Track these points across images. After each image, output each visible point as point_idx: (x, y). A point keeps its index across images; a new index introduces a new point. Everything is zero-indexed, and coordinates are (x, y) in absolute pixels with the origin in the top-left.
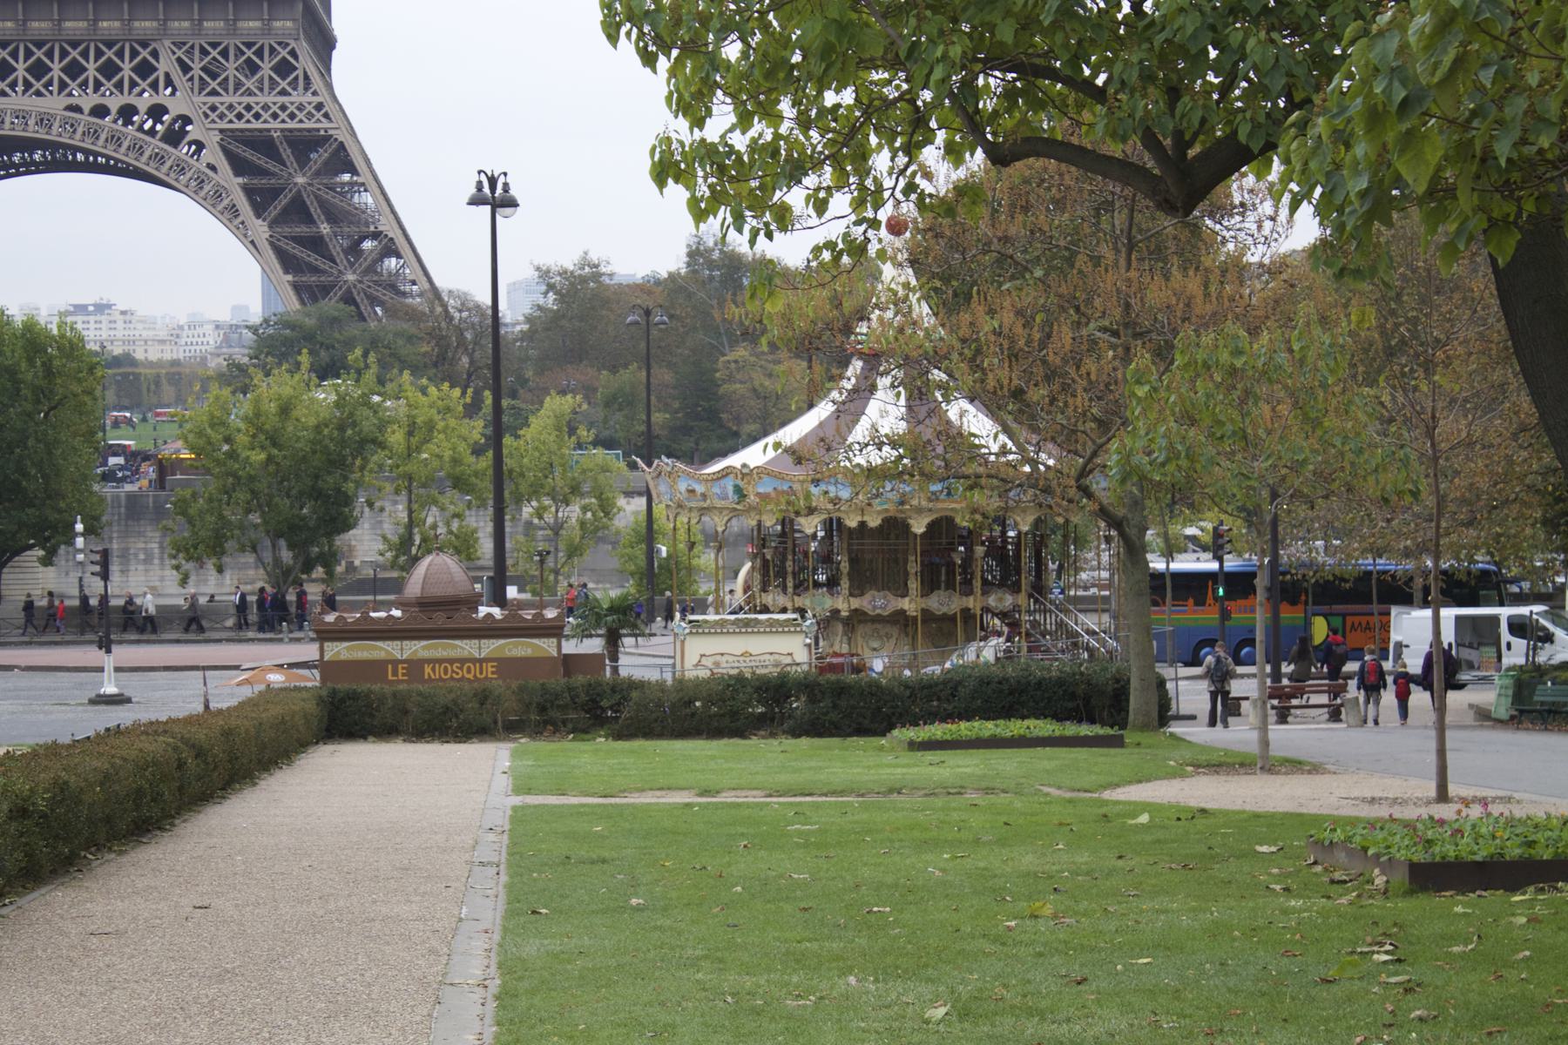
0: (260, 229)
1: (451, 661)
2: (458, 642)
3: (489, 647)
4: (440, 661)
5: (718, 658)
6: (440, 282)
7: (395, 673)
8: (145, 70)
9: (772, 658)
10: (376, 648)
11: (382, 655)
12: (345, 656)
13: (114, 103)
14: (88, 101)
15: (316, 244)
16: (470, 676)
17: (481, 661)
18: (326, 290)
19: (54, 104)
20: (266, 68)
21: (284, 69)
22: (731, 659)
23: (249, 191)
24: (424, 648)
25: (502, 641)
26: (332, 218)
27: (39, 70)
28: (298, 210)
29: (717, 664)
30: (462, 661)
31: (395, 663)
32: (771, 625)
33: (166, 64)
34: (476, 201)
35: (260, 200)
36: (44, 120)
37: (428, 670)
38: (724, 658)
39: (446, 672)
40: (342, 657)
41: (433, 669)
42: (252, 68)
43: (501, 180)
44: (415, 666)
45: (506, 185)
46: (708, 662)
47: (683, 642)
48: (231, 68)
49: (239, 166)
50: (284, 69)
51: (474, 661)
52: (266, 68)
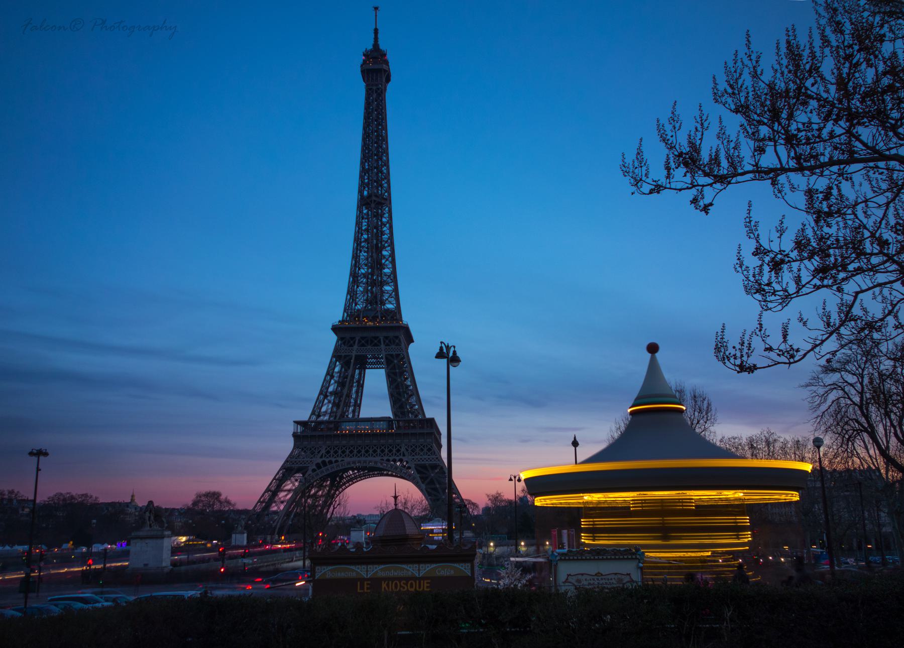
0: (423, 486)
1: (400, 579)
2: (404, 566)
3: (425, 569)
4: (393, 579)
5: (580, 577)
6: (463, 497)
7: (362, 587)
8: (398, 451)
9: (616, 577)
10: (353, 571)
11: (354, 575)
12: (329, 576)
13: (391, 458)
14: (385, 458)
15: (435, 489)
16: (413, 590)
17: (420, 579)
18: (438, 500)
19: (378, 459)
20: (425, 450)
21: (429, 450)
22: (588, 578)
23: (421, 478)
24: (382, 570)
25: (434, 565)
26: (439, 484)
27: (375, 451)
28: (432, 482)
29: (579, 581)
30: (407, 579)
31: (362, 580)
32: (615, 554)
33: (403, 450)
34: (440, 355)
35: (423, 479)
36: (376, 462)
37: (384, 585)
38: (584, 577)
39: (396, 587)
40: (327, 577)
41: (388, 585)
42: (422, 450)
43: (452, 349)
44: (376, 582)
45: (454, 352)
46: (573, 580)
47: (556, 565)
48: (418, 450)
49: (419, 472)
50: (429, 450)
51: (414, 578)
52: (425, 450)
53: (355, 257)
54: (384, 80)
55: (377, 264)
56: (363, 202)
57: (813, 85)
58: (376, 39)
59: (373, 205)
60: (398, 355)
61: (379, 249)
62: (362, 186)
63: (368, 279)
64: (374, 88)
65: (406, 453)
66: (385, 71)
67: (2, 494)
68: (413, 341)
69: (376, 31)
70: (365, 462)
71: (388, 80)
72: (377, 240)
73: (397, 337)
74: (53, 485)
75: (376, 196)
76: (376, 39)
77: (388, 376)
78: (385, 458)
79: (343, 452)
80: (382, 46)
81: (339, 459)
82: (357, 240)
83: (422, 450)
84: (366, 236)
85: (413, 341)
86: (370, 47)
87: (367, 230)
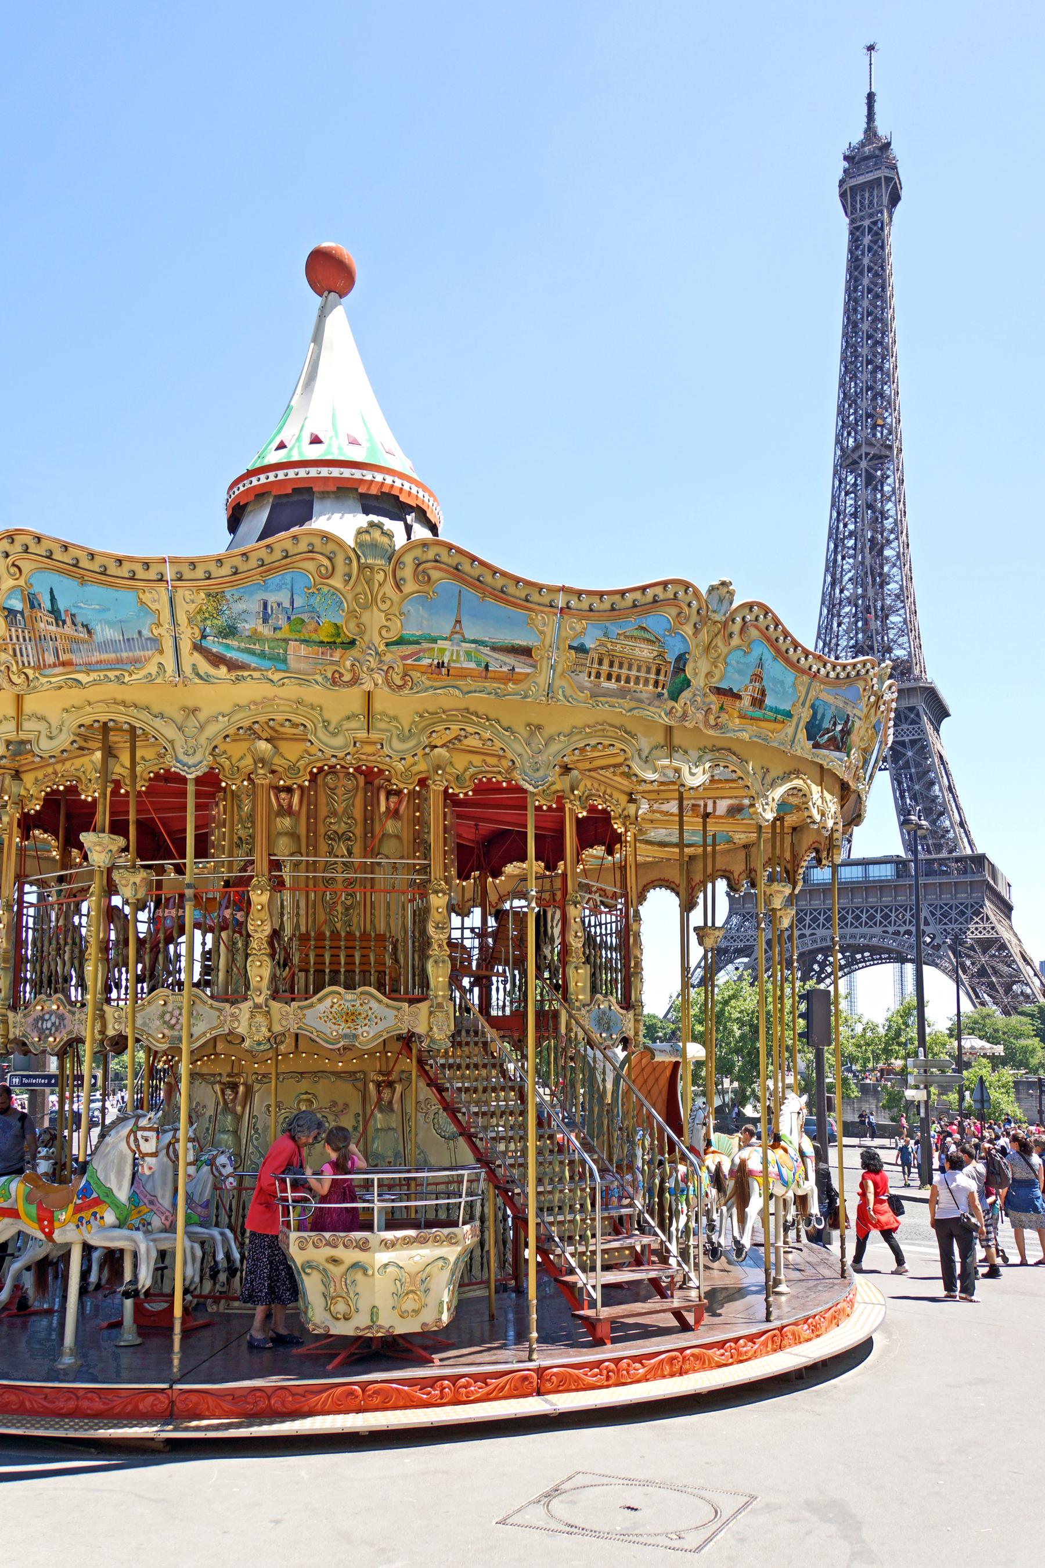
14: (891, 929)
19: (878, 930)
48: (953, 914)
53: (832, 567)
54: (885, 200)
55: (873, 576)
56: (847, 461)
57: (123, 1098)
58: (871, 117)
59: (863, 464)
60: (913, 742)
61: (877, 548)
62: (845, 426)
63: (856, 606)
64: (866, 223)
65: (930, 919)
66: (889, 180)
67: (50, 594)
68: (948, 715)
69: (871, 97)
70: (853, 936)
71: (895, 199)
72: (875, 531)
73: (912, 709)
74: (542, 944)
75: (871, 444)
76: (871, 117)
77: (893, 779)
78: (891, 929)
79: (815, 920)
80: (883, 129)
81: (807, 932)
82: (836, 538)
83: (962, 913)
84: (851, 527)
85: (948, 715)
86: (858, 136)
87: (854, 515)
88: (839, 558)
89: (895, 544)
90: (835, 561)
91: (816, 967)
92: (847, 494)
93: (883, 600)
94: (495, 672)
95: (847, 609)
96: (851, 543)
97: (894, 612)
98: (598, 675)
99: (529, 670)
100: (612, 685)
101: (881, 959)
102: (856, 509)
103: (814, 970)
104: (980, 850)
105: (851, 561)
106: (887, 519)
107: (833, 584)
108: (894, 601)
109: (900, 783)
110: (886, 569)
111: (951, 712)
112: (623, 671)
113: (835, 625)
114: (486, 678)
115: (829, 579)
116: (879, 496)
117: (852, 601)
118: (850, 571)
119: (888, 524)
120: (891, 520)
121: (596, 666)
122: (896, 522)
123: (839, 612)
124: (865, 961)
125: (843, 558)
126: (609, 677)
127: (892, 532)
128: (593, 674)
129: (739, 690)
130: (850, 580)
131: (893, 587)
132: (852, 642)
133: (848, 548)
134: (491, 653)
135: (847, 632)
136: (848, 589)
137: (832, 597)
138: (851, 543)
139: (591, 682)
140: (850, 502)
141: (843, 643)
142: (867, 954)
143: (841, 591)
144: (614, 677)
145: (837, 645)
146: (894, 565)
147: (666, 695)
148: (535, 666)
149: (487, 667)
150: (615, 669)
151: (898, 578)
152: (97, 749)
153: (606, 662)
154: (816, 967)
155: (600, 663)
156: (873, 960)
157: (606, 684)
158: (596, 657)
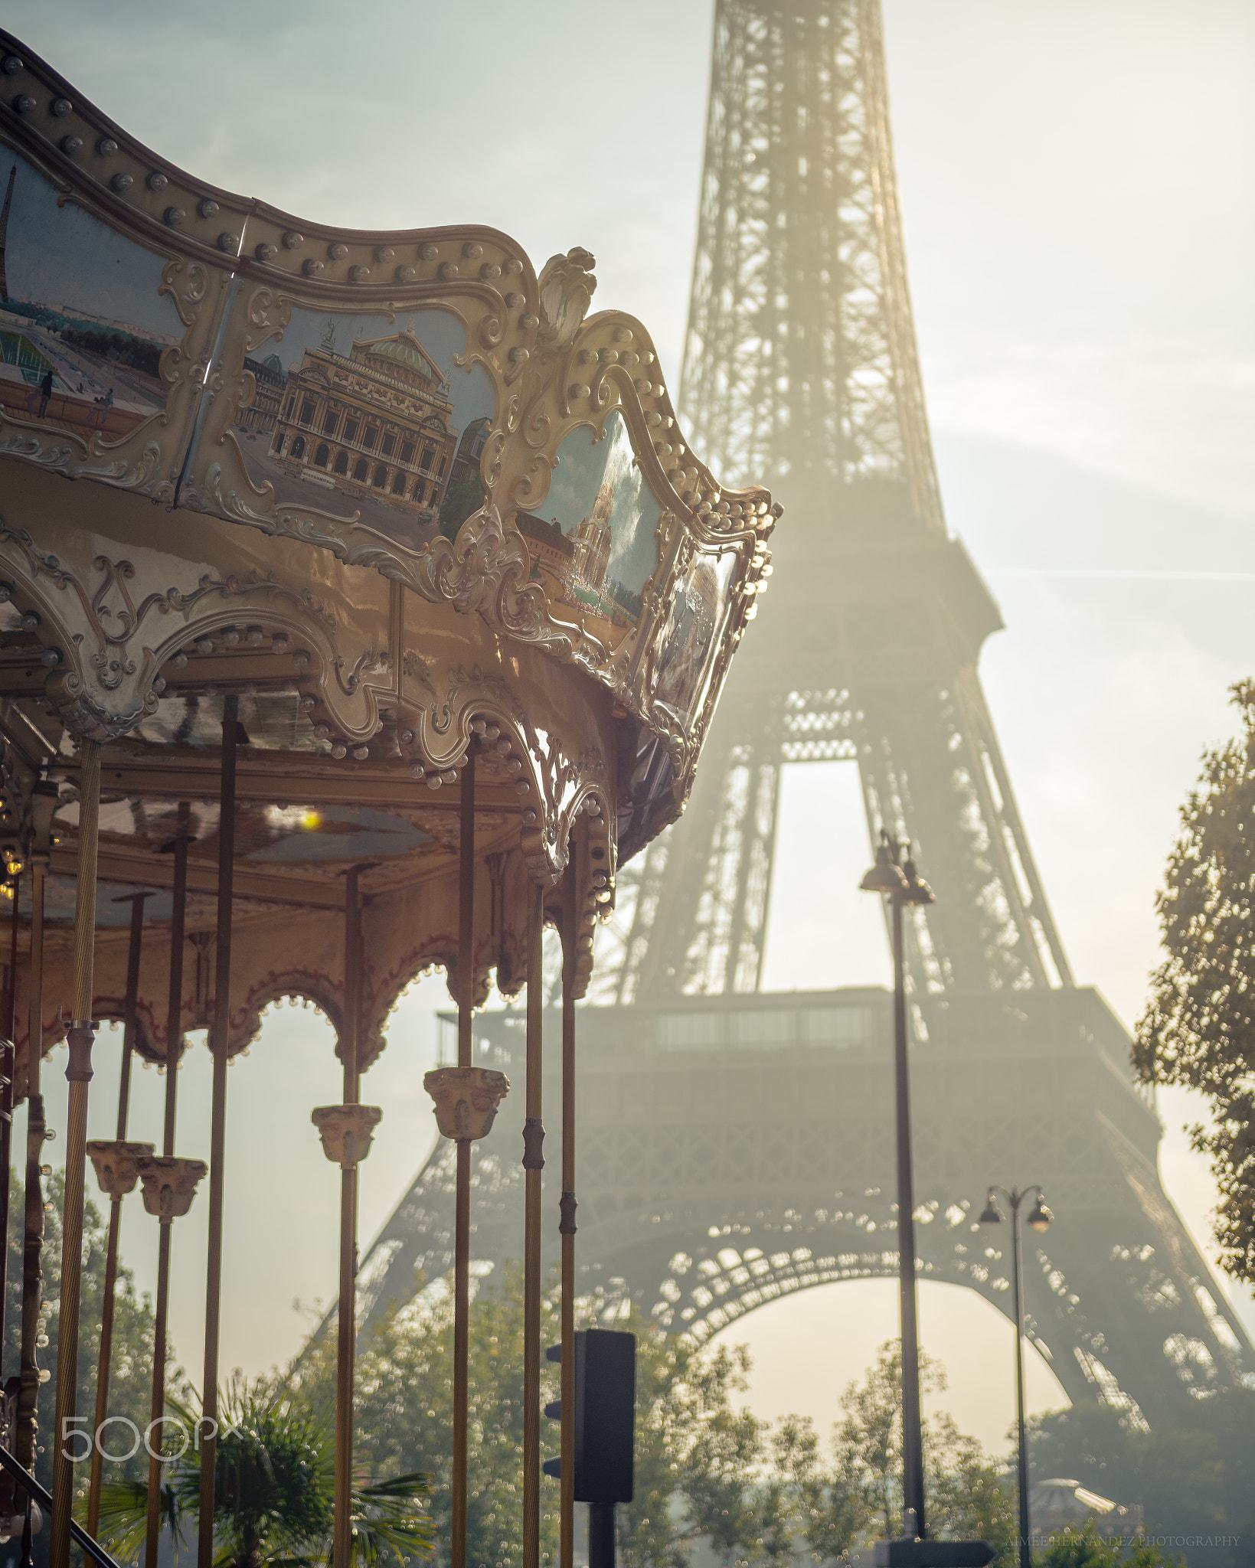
68: (997, 625)
82: (719, 160)
88: (732, 216)
89: (863, 195)
90: (721, 221)
91: (669, 1289)
92: (750, 61)
93: (838, 328)
94: (66, 400)
95: (751, 345)
96: (759, 182)
97: (865, 359)
98: (297, 450)
99: (149, 410)
100: (325, 478)
101: (838, 1267)
102: (771, 102)
103: (662, 1298)
104: (1081, 980)
105: (760, 225)
106: (844, 131)
107: (718, 278)
108: (863, 331)
109: (884, 796)
110: (844, 252)
111: (1006, 614)
112: (354, 445)
113: (722, 381)
114: (41, 414)
115: (706, 265)
116: (824, 76)
117: (763, 323)
118: (757, 250)
119: (849, 143)
120: (854, 136)
121: (295, 422)
122: (866, 143)
123: (731, 348)
124: (797, 1274)
125: (742, 217)
126: (321, 459)
127: (856, 162)
128: (287, 443)
129: (570, 534)
130: (759, 271)
131: (861, 298)
132: (764, 428)
133: (754, 194)
134: (62, 349)
135: (755, 398)
136: (753, 296)
137: (714, 313)
138: (759, 182)
139: (281, 461)
140: (756, 84)
141: (742, 428)
142: (802, 1254)
143: (737, 300)
144: (332, 457)
145: (727, 432)
146: (863, 245)
147: (435, 523)
148: (160, 401)
149: (47, 382)
150: (337, 437)
151: (873, 278)
152: (147, 928)
153: (320, 415)
154: (669, 1289)
155: (307, 418)
156: (817, 1270)
157: (312, 475)
158: (300, 397)
